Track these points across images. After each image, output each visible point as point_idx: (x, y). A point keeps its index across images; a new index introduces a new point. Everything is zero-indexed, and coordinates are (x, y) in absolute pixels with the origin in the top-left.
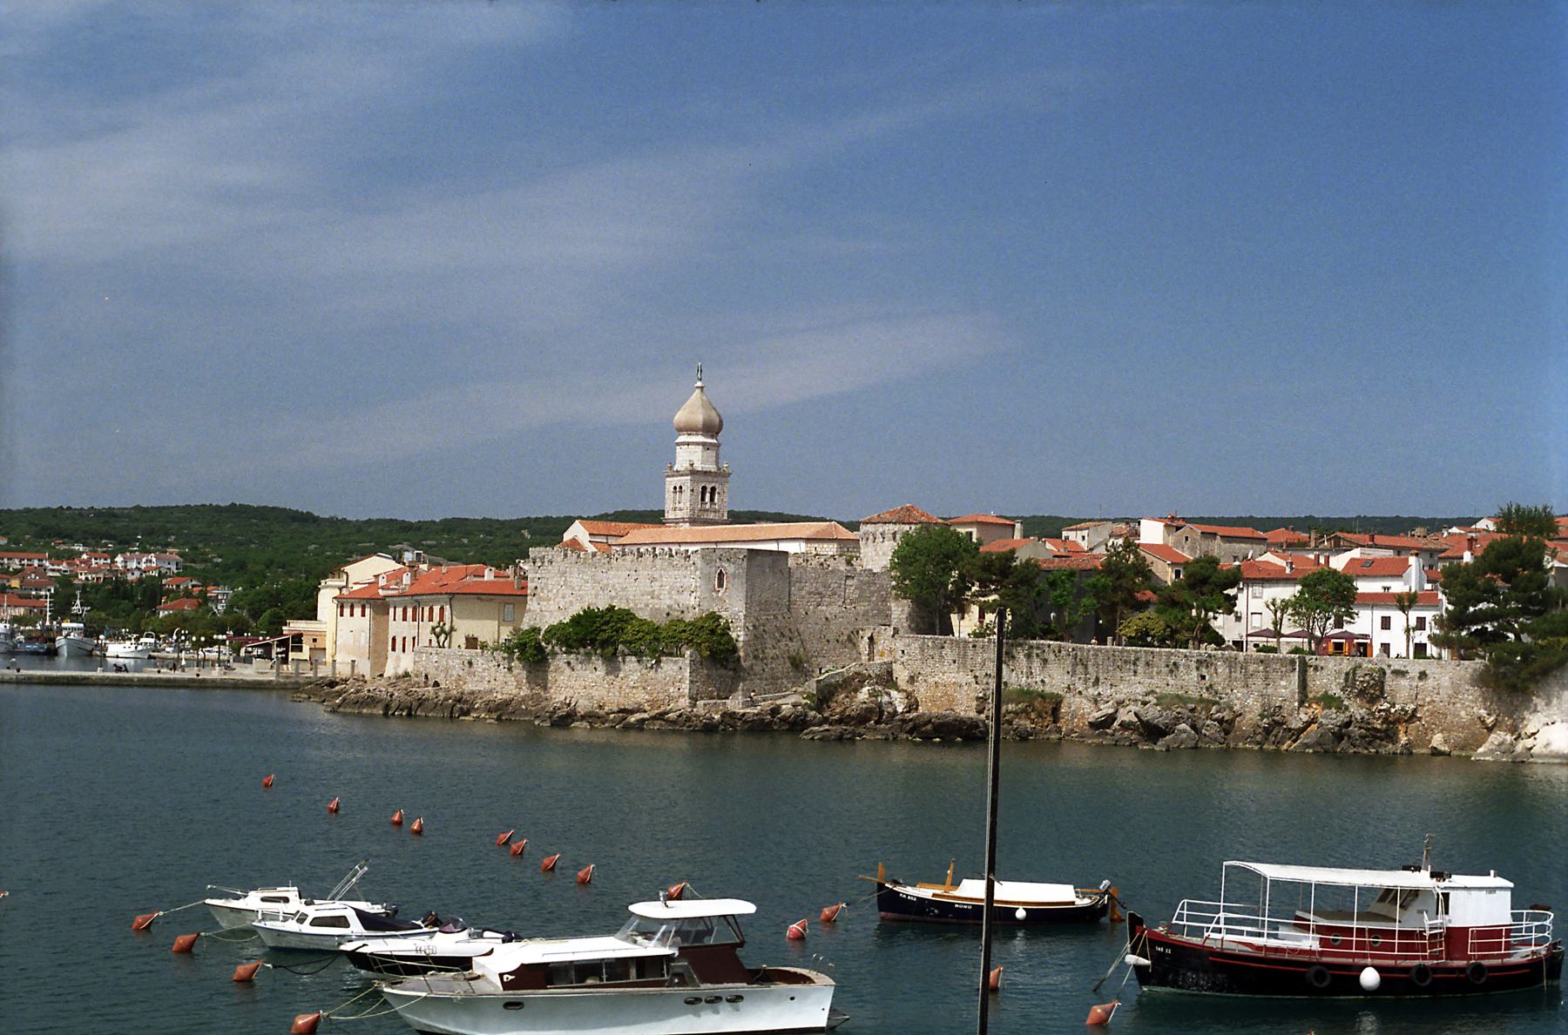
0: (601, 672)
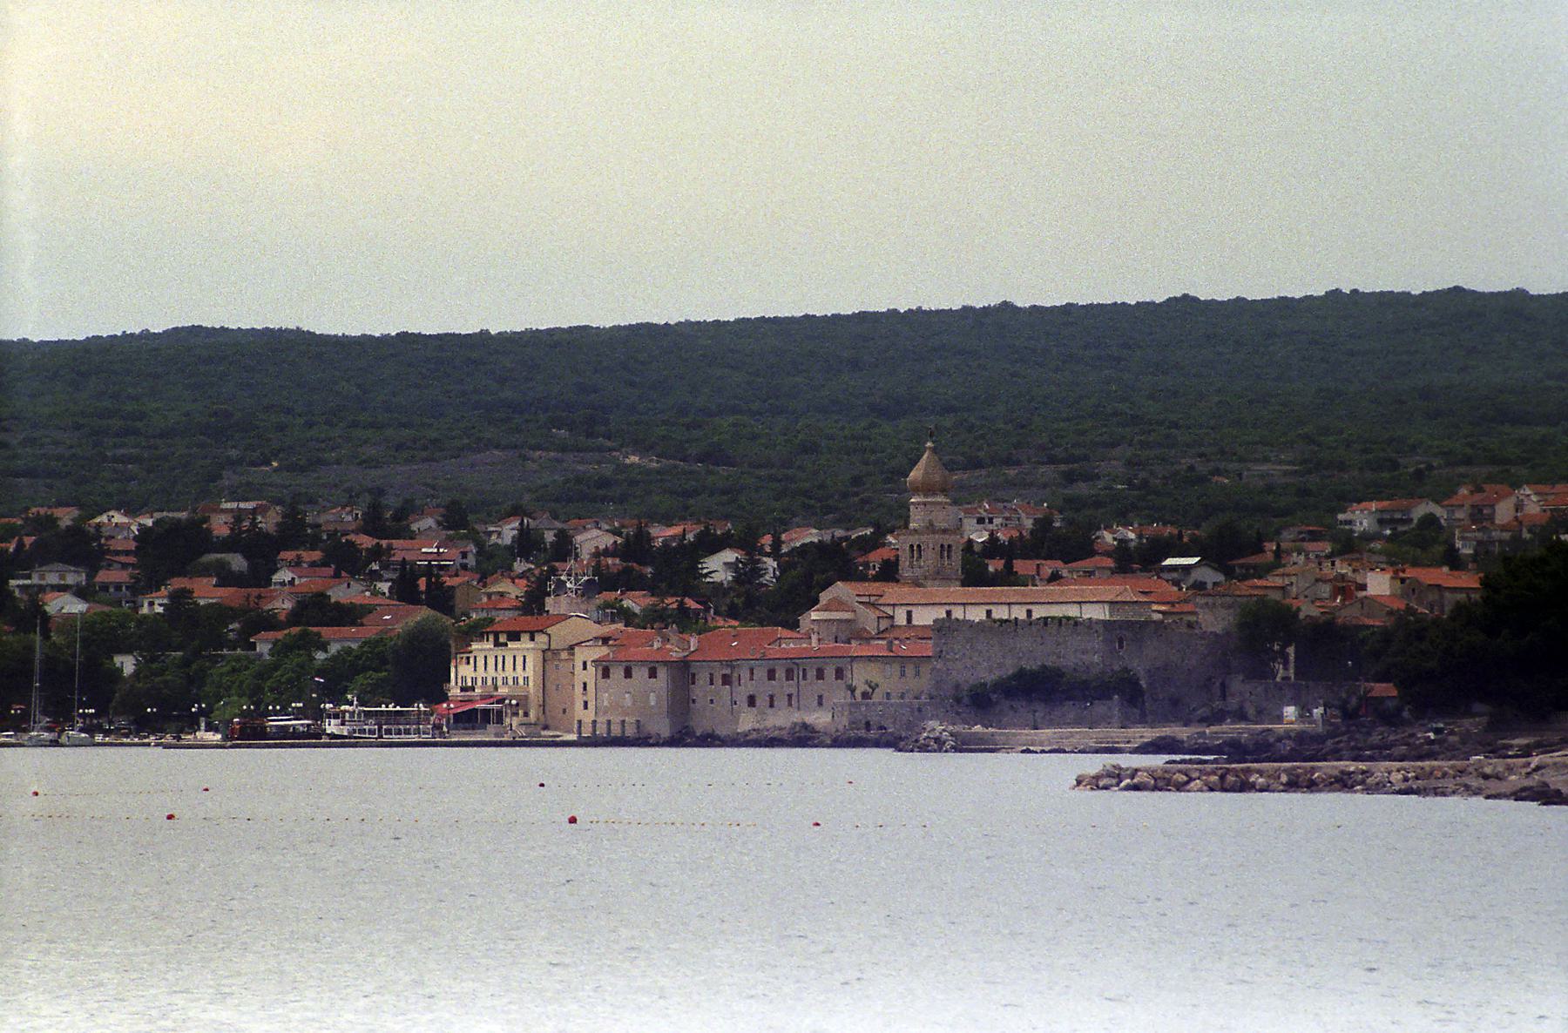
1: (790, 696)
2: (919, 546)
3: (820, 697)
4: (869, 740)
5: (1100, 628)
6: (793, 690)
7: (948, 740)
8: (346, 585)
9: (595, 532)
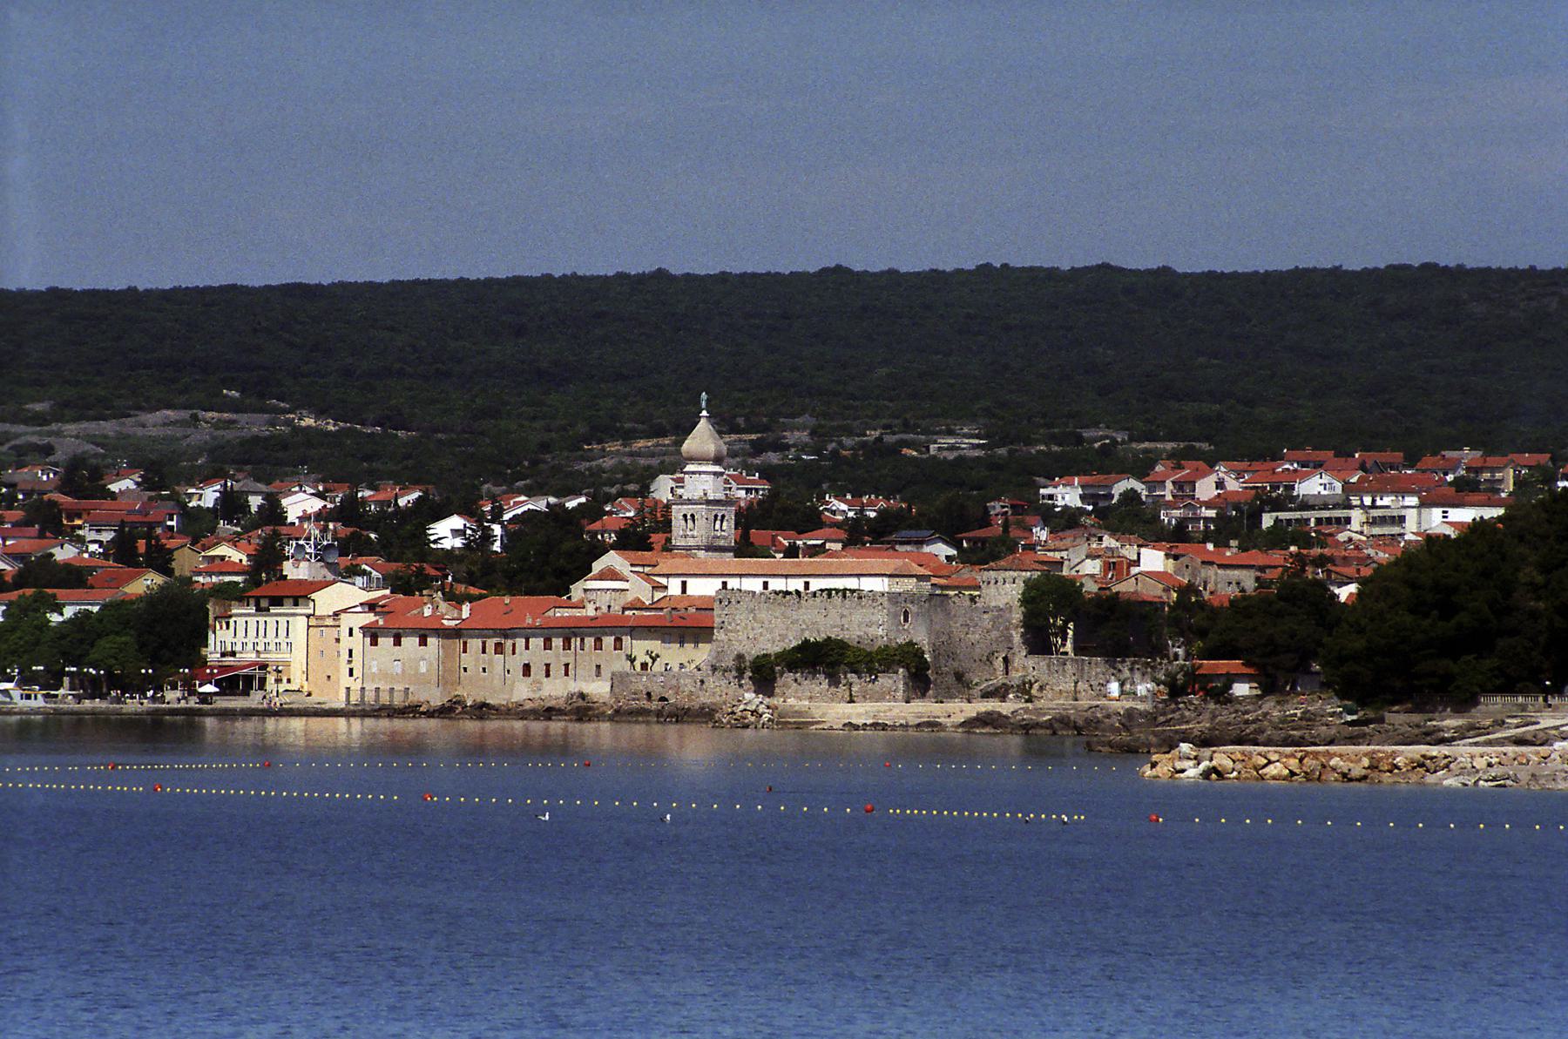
0: (825, 685)
1: (567, 665)
2: (692, 516)
3: (598, 667)
4: (651, 711)
5: (885, 600)
6: (571, 660)
7: (765, 713)
8: (1319, 476)
9: (301, 496)
